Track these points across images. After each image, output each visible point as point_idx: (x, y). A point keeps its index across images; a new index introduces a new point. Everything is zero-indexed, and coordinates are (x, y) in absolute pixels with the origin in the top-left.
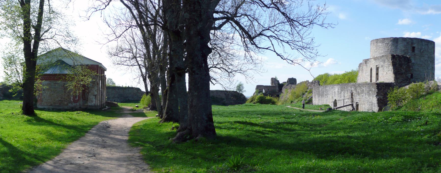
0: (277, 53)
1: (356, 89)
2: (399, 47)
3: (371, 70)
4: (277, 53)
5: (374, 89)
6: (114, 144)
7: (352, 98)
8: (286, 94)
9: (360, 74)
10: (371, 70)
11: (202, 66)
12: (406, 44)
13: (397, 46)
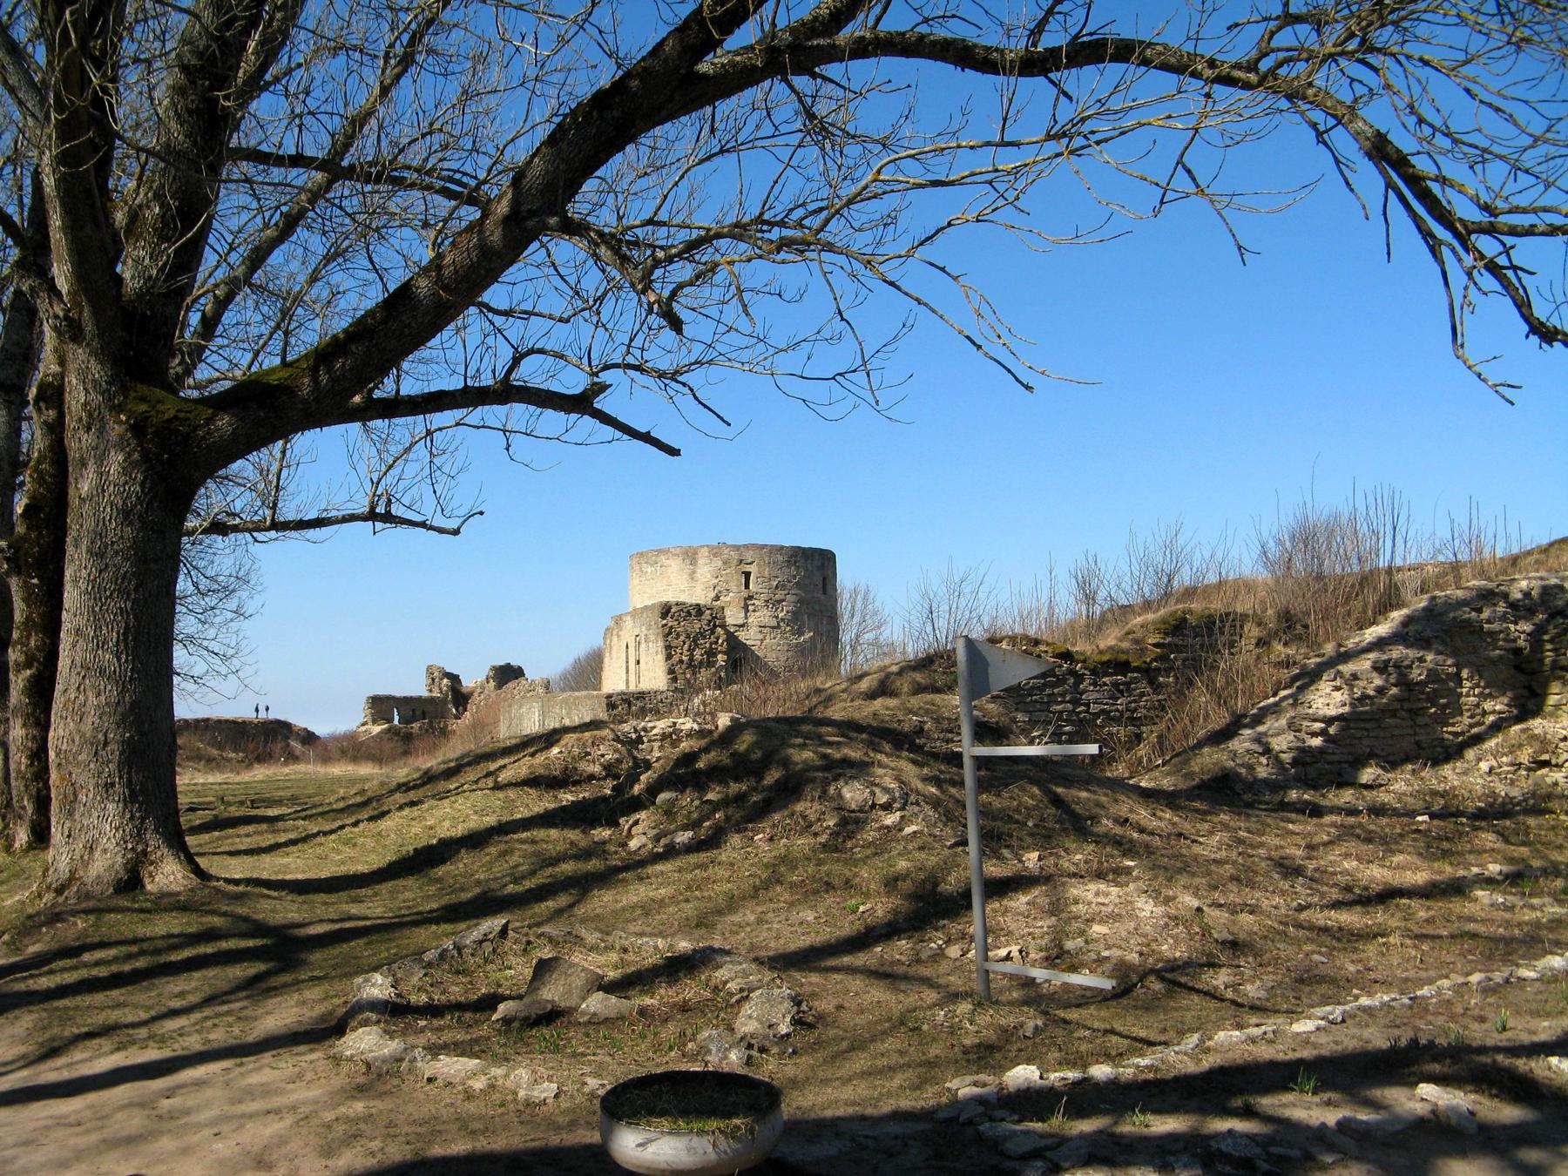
2: (698, 575)
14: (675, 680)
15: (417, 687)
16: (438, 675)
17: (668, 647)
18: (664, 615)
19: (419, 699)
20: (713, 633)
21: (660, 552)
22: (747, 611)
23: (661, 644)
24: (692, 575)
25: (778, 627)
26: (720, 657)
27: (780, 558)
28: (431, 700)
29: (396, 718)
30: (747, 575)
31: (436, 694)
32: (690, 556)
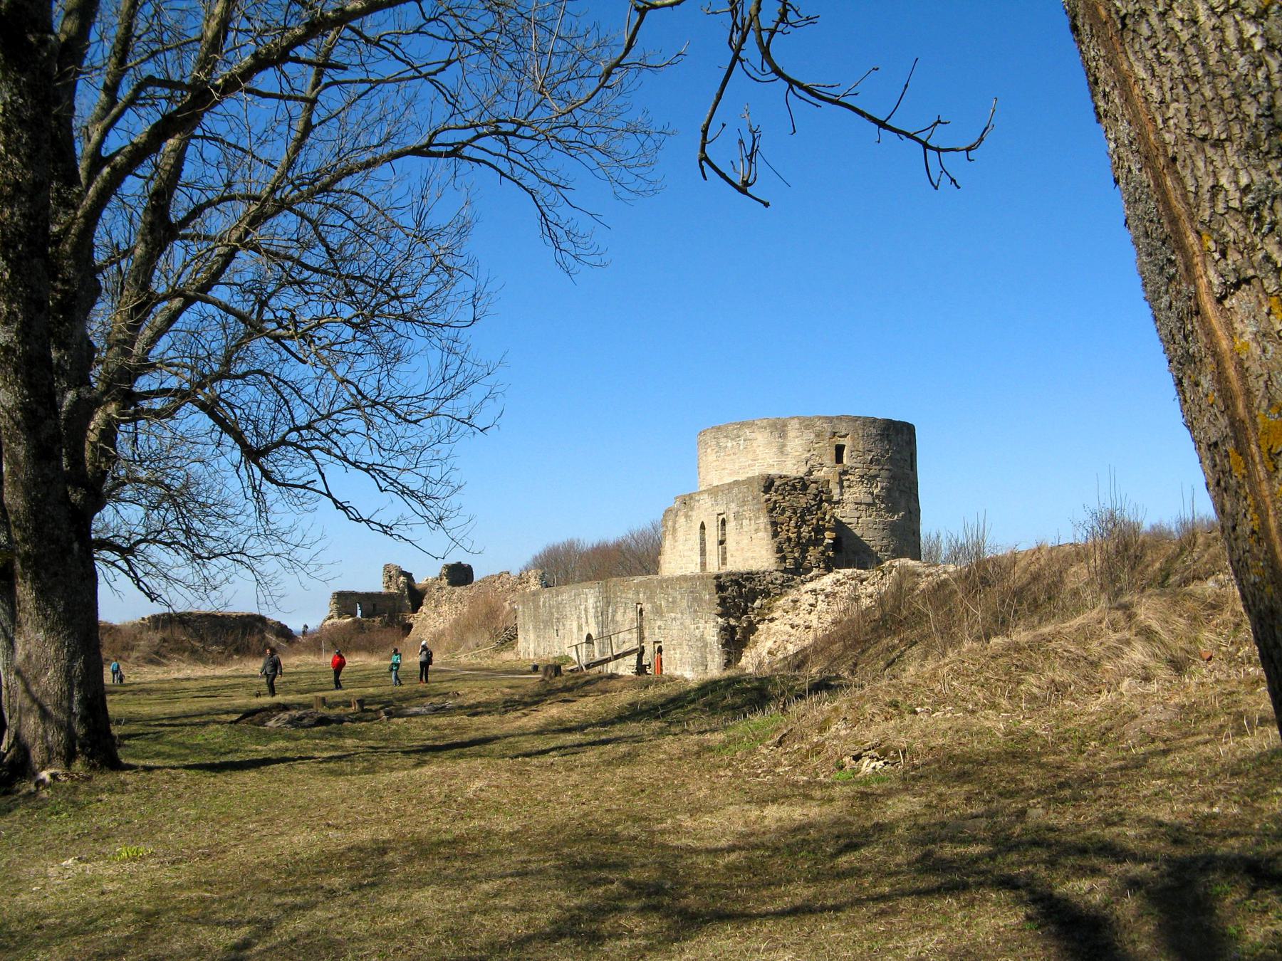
0: (335, 501)
1: (650, 599)
2: (788, 449)
3: (703, 527)
4: (335, 501)
5: (709, 596)
6: (600, 667)
7: (640, 629)
8: (431, 622)
9: (667, 544)
10: (703, 527)
11: (71, 551)
12: (812, 436)
13: (784, 446)
14: (783, 559)
15: (374, 583)
16: (392, 573)
17: (774, 524)
18: (767, 489)
19: (379, 595)
20: (819, 508)
21: (743, 424)
22: (842, 487)
23: (764, 520)
24: (781, 449)
25: (874, 504)
26: (827, 534)
27: (874, 431)
28: (390, 596)
29: (359, 612)
30: (839, 450)
31: (393, 590)
32: (779, 429)
